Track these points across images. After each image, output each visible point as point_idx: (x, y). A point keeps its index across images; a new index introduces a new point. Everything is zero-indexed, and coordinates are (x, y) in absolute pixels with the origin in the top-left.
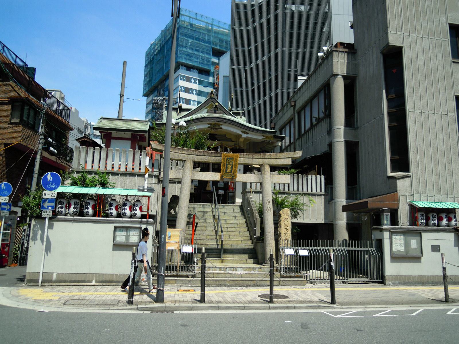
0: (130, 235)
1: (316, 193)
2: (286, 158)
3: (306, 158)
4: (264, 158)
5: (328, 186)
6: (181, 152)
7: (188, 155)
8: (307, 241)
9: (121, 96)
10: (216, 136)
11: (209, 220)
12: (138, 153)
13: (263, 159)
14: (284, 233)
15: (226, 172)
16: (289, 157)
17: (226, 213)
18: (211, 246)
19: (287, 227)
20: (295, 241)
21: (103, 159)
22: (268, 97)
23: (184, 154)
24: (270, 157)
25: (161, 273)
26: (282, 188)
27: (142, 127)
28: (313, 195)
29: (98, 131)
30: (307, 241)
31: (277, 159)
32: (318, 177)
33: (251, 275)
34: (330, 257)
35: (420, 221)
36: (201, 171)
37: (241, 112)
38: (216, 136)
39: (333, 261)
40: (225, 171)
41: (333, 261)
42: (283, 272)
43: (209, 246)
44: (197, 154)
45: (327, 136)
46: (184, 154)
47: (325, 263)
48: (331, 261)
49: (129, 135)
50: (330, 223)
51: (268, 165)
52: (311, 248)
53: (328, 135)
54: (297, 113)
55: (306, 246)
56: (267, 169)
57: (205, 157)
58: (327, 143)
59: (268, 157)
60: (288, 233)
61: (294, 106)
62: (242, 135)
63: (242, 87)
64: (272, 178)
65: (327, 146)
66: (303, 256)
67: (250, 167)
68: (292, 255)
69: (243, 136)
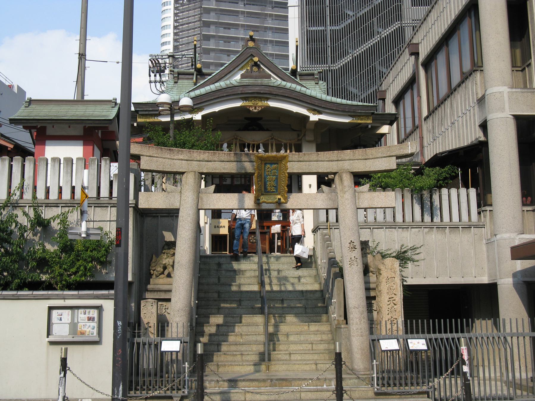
0: (78, 322)
1: (460, 224)
2: (384, 157)
3: (436, 154)
4: (301, 159)
5: (483, 209)
6: (175, 157)
7: (189, 162)
8: (414, 321)
9: (82, 56)
10: (260, 122)
11: (246, 286)
12: (94, 164)
13: (337, 160)
14: (389, 306)
15: (265, 192)
16: (392, 154)
17: (280, 270)
18: (247, 337)
19: (393, 296)
20: (411, 324)
21: (29, 178)
22: (376, 39)
23: (182, 160)
24: (352, 158)
25: (118, 396)
26: (389, 218)
27: (103, 114)
28: (454, 228)
29: (21, 127)
30: (414, 321)
31: (366, 159)
32: (463, 191)
33: (320, 393)
34: (462, 355)
35: (335, 315)
36: (217, 191)
37: (316, 72)
38: (260, 122)
39: (467, 362)
40: (263, 189)
41: (467, 362)
42: (378, 385)
43: (244, 337)
44: (206, 159)
45: (476, 108)
46: (182, 160)
47: (452, 364)
48: (464, 363)
49: (78, 131)
50: (491, 282)
51: (348, 174)
52: (433, 336)
53: (479, 107)
54: (422, 65)
55: (423, 332)
56: (348, 180)
57: (223, 163)
58: (477, 124)
59: (347, 158)
60: (395, 307)
61: (416, 54)
62: (308, 117)
63: (324, 24)
64: (359, 198)
65: (478, 128)
66: (416, 352)
67: (326, 178)
68: (396, 350)
69: (311, 119)
